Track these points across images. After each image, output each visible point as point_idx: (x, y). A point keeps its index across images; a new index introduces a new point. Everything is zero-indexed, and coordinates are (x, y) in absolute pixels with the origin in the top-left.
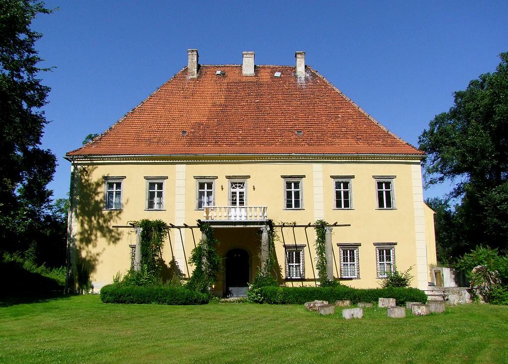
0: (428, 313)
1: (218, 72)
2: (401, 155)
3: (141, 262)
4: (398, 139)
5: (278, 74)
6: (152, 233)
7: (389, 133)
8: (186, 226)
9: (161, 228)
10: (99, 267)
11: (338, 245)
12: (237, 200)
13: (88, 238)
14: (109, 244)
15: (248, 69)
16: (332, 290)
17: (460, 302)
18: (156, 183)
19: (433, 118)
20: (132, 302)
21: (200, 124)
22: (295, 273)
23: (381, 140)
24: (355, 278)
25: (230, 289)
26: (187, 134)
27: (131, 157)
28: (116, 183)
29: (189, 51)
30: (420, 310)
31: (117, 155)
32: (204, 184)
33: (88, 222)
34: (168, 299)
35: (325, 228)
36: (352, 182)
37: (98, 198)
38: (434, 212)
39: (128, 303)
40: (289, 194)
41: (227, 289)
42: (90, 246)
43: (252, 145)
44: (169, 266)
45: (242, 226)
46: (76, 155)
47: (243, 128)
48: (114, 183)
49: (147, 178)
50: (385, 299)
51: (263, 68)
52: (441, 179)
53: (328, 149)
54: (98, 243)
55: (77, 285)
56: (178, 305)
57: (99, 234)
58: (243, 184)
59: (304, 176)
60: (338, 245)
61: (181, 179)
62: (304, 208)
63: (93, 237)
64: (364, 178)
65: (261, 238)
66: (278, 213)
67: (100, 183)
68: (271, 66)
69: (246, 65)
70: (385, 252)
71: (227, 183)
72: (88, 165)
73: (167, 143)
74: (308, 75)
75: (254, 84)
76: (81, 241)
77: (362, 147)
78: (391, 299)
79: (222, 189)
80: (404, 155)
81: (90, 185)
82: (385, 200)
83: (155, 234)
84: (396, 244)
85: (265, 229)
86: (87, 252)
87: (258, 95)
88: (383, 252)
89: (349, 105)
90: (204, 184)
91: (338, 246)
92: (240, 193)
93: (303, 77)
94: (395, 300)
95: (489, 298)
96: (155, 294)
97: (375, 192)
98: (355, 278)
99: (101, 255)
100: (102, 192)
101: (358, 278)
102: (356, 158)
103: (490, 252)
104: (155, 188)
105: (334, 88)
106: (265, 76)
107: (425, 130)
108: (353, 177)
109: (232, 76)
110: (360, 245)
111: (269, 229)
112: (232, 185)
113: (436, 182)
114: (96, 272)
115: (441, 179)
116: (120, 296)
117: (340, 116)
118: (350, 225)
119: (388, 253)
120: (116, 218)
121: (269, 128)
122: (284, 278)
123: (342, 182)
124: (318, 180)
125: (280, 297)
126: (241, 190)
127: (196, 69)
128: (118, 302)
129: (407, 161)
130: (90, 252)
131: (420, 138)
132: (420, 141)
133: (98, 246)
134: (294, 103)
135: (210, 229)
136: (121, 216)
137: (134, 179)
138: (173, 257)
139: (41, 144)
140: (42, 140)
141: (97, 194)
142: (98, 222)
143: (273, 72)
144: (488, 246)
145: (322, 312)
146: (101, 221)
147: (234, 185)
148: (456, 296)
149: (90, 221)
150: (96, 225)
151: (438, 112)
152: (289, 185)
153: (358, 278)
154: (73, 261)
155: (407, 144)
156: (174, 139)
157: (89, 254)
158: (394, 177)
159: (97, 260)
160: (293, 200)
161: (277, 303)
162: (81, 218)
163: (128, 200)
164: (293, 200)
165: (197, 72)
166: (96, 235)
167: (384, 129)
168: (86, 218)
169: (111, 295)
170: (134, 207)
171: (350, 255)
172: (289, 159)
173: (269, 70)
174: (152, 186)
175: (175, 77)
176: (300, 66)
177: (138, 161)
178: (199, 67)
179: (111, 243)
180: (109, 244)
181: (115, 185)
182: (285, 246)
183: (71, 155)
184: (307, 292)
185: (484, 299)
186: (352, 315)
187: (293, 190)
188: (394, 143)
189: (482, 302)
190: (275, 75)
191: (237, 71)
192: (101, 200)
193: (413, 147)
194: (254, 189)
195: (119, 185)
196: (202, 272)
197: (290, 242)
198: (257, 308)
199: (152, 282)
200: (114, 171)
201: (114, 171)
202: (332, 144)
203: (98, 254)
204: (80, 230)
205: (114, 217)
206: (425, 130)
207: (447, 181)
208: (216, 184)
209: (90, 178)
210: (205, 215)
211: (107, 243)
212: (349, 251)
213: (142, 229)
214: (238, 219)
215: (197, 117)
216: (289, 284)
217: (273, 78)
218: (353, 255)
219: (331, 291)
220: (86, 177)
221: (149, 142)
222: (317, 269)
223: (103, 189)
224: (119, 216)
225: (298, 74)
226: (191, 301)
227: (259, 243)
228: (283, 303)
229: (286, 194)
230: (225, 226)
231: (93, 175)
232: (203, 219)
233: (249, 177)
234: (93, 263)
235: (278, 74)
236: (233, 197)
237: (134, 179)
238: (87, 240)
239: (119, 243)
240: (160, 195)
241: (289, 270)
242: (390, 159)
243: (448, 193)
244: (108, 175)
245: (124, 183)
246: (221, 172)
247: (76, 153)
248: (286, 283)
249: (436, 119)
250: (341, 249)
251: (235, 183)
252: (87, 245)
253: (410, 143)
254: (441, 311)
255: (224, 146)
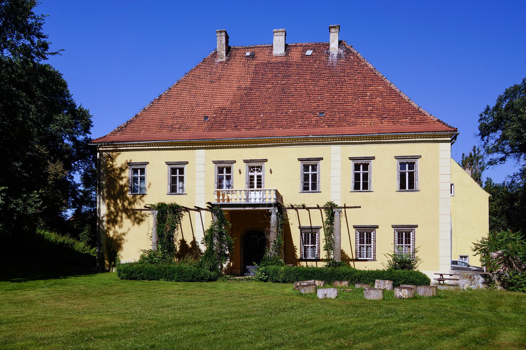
0: (411, 296)
1: (248, 54)
2: (428, 133)
3: (157, 242)
4: (429, 116)
5: (309, 52)
6: (168, 216)
7: (420, 109)
8: (304, 207)
9: (176, 211)
10: (125, 246)
11: (355, 227)
12: (255, 183)
13: (114, 219)
14: (134, 225)
15: (279, 50)
16: (333, 270)
17: (472, 287)
18: (138, 169)
19: (502, 92)
20: (143, 279)
21: (223, 109)
22: (365, 254)
23: (409, 118)
24: (371, 260)
25: (248, 267)
26: (209, 119)
27: (152, 144)
28: (140, 169)
29: (218, 32)
30: (421, 291)
31: (139, 141)
32: (223, 168)
33: (114, 205)
34: (176, 276)
35: (334, 210)
36: (418, 162)
37: (122, 183)
38: (489, 195)
39: (139, 280)
40: (306, 177)
41: (245, 267)
42: (117, 227)
43: (271, 128)
44: (190, 246)
45: (251, 208)
46: (100, 143)
47: (265, 111)
48: (139, 169)
49: (168, 164)
50: (381, 281)
51: (295, 46)
52: (503, 159)
53: (348, 130)
54: (123, 224)
55: (107, 262)
56: (186, 281)
57: (124, 215)
58: (261, 167)
59: (322, 159)
60: (355, 227)
61: (200, 165)
62: (320, 191)
63: (119, 219)
64: (385, 159)
65: (270, 219)
66: (293, 195)
67: (124, 168)
68: (304, 44)
69: (277, 45)
70: (404, 234)
71: (244, 167)
72: (112, 151)
73: (188, 128)
74: (342, 51)
75: (285, 64)
76: (108, 222)
77: (387, 126)
78: (387, 281)
79: (240, 172)
80: (431, 133)
81: (114, 170)
82: (407, 180)
83: (169, 216)
84: (416, 226)
85: (274, 211)
86: (114, 232)
87: (286, 76)
88: (309, 235)
89: (381, 81)
90: (223, 168)
91: (354, 228)
92: (258, 176)
93: (336, 54)
94: (391, 282)
95: (508, 285)
96: (164, 272)
97: (397, 174)
98: (371, 260)
99: (126, 235)
100: (126, 177)
101: (374, 260)
102: (377, 138)
103: (512, 235)
104: (177, 173)
105: (368, 63)
106: (295, 55)
107: (488, 107)
108: (373, 158)
109: (262, 57)
110: (377, 227)
111: (277, 211)
112: (250, 169)
113: (496, 163)
114: (122, 250)
115: (503, 159)
116: (132, 273)
117: (368, 94)
118: (360, 207)
119: (408, 235)
120: (140, 200)
121: (291, 111)
122: (299, 257)
123: (362, 163)
124: (336, 162)
125: (282, 276)
126: (259, 174)
127: (225, 52)
128: (131, 279)
129: (435, 139)
130: (117, 232)
131: (481, 115)
132: (481, 119)
133: (124, 227)
134: (321, 83)
135: (221, 211)
136: (145, 198)
137: (157, 165)
138: (194, 237)
139: (90, 133)
140: (91, 130)
141: (122, 179)
142: (123, 205)
143: (305, 51)
144: (509, 229)
145: (302, 291)
146: (126, 204)
147: (251, 169)
148: (467, 280)
149: (116, 204)
150: (121, 208)
151: (509, 84)
152: (306, 168)
153: (374, 260)
154: (103, 242)
155: (438, 121)
156: (195, 124)
157: (116, 234)
158: (146, 163)
159: (123, 239)
160: (310, 183)
161: (278, 282)
162: (107, 201)
163: (150, 184)
164: (310, 183)
165: (227, 54)
166: (122, 217)
167: (415, 105)
168: (113, 201)
169: (124, 272)
170: (157, 190)
171: (367, 237)
172: (305, 141)
173: (301, 49)
174: (173, 171)
175: (204, 61)
176: (333, 41)
177: (160, 147)
178: (228, 49)
179: (136, 224)
180: (134, 225)
181: (139, 171)
182: (300, 227)
183: (95, 143)
184: (308, 272)
185: (502, 285)
186: (325, 295)
187: (310, 172)
188: (424, 119)
189: (499, 288)
190: (306, 54)
191: (267, 51)
192: (125, 184)
193: (444, 124)
194: (271, 172)
195: (143, 171)
196: (213, 252)
197: (305, 223)
198: (264, 286)
199: (170, 260)
200: (137, 157)
201: (137, 157)
202: (354, 124)
203: (123, 234)
204: (107, 213)
205: (137, 200)
206: (488, 107)
207: (511, 161)
208: (235, 168)
209: (114, 164)
210: (216, 198)
211: (132, 224)
212: (366, 234)
213: (157, 212)
214: (238, 202)
215: (220, 102)
216: (304, 264)
217: (304, 56)
218: (370, 237)
219: (338, 271)
220: (111, 163)
221: (172, 128)
222: (325, 250)
223: (127, 174)
224: (142, 199)
225: (331, 50)
226: (198, 279)
227: (269, 225)
228: (284, 282)
229: (353, 176)
230: (235, 209)
231: (116, 160)
232: (214, 202)
233: (266, 160)
234: (120, 242)
235: (309, 52)
236: (251, 180)
237: (157, 165)
238: (113, 221)
239: (143, 224)
240: (182, 179)
241: (360, 250)
242: (415, 138)
243: (512, 175)
244: (131, 160)
245: (147, 168)
246: (239, 156)
247: (101, 141)
248: (301, 263)
249: (506, 93)
250: (357, 231)
251: (253, 167)
252: (114, 226)
253: (441, 120)
254: (431, 295)
255: (243, 130)
